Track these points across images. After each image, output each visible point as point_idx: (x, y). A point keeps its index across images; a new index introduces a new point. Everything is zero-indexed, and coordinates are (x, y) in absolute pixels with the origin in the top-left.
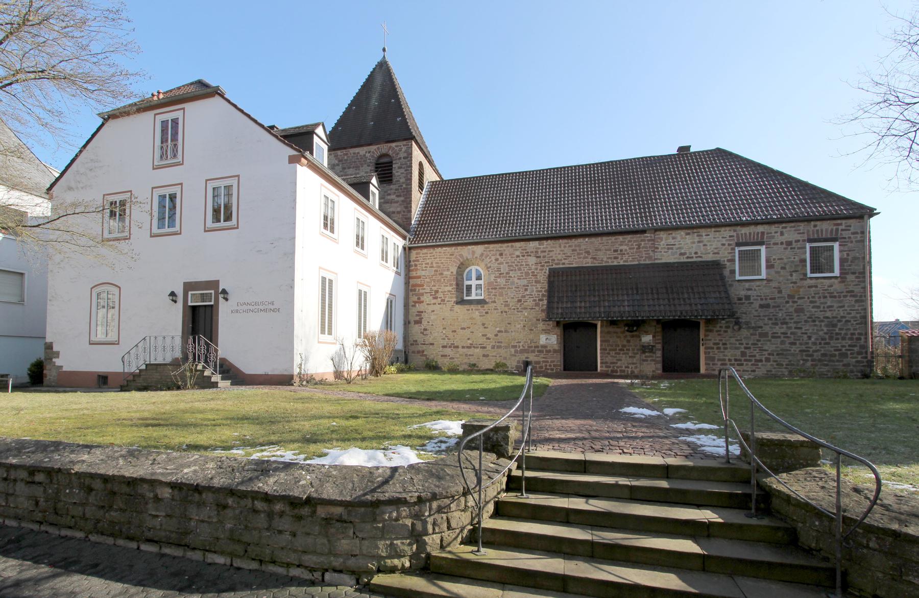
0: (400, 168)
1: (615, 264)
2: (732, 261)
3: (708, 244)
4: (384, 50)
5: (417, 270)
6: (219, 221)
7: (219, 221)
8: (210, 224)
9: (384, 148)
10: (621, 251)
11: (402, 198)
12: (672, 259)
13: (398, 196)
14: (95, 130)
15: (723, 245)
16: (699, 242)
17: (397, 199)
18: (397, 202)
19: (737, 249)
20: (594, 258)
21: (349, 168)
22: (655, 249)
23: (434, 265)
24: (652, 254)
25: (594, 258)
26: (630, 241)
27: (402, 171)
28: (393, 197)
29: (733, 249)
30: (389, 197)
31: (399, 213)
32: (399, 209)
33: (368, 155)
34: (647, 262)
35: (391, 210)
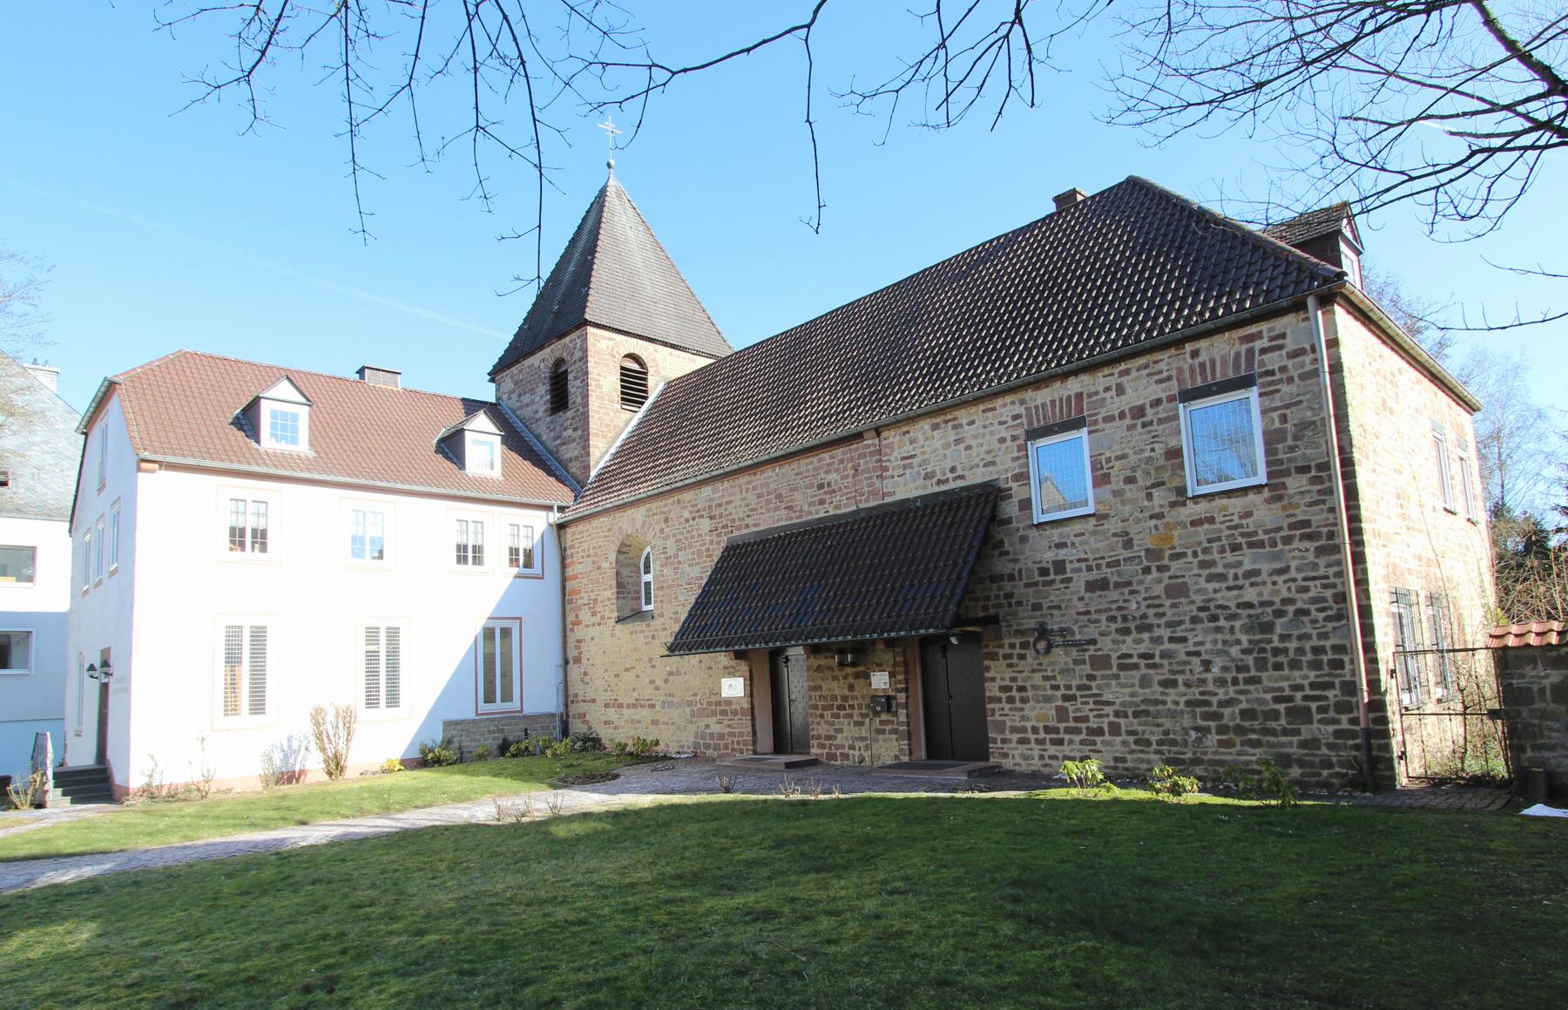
1: (822, 515)
10: (829, 484)
15: (1003, 440)
24: (878, 484)
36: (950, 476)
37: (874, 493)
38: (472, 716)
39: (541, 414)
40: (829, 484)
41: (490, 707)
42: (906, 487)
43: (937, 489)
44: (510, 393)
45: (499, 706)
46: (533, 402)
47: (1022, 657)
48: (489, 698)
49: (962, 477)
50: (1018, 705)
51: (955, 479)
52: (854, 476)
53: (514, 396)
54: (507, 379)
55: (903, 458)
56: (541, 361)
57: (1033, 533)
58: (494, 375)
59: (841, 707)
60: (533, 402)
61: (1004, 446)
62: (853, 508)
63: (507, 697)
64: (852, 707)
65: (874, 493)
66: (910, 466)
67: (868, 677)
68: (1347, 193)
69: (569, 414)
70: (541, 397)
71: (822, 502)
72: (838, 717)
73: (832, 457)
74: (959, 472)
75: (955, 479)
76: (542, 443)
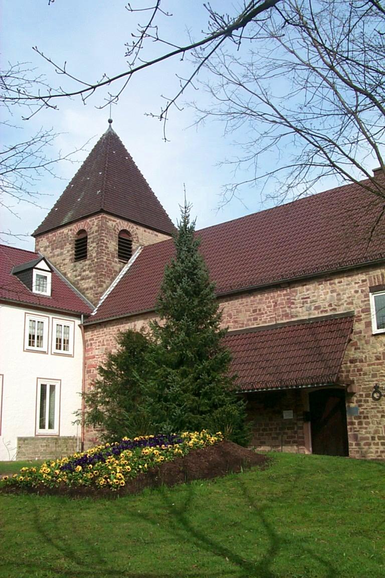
0: (92, 242)
1: (255, 326)
2: (367, 310)
3: (341, 293)
4: (110, 121)
5: (92, 349)
6: (60, 349)
7: (60, 349)
8: (27, 347)
9: (81, 225)
10: (260, 310)
11: (94, 273)
12: (304, 316)
13: (90, 272)
14: (42, 268)
15: (356, 292)
16: (332, 292)
17: (90, 274)
18: (90, 278)
19: (372, 297)
20: (236, 322)
21: (57, 248)
22: (291, 303)
23: (105, 343)
24: (288, 310)
25: (236, 322)
26: (267, 298)
27: (94, 245)
28: (87, 272)
29: (367, 296)
30: (84, 274)
31: (91, 288)
32: (91, 285)
33: (70, 232)
34: (285, 321)
35: (85, 286)
36: (329, 309)
37: (287, 315)
38: (33, 435)
39: (67, 261)
40: (260, 310)
41: (42, 431)
42: (303, 314)
43: (320, 315)
44: (46, 247)
45: (46, 431)
46: (62, 254)
47: (367, 401)
48: (42, 426)
49: (335, 309)
50: (364, 426)
51: (331, 310)
52: (275, 306)
53: (49, 249)
54: (44, 241)
55: (302, 299)
56: (70, 232)
57: (372, 339)
58: (37, 235)
59: (264, 430)
60: (62, 254)
61: (357, 295)
62: (274, 323)
63: (51, 426)
64: (271, 430)
65: (287, 315)
66: (306, 302)
67: (282, 413)
68: (368, 285)
69: (87, 262)
70: (69, 250)
71: (255, 319)
72: (263, 435)
73: (229, 304)
74: (334, 307)
75: (331, 310)
76: (67, 278)
